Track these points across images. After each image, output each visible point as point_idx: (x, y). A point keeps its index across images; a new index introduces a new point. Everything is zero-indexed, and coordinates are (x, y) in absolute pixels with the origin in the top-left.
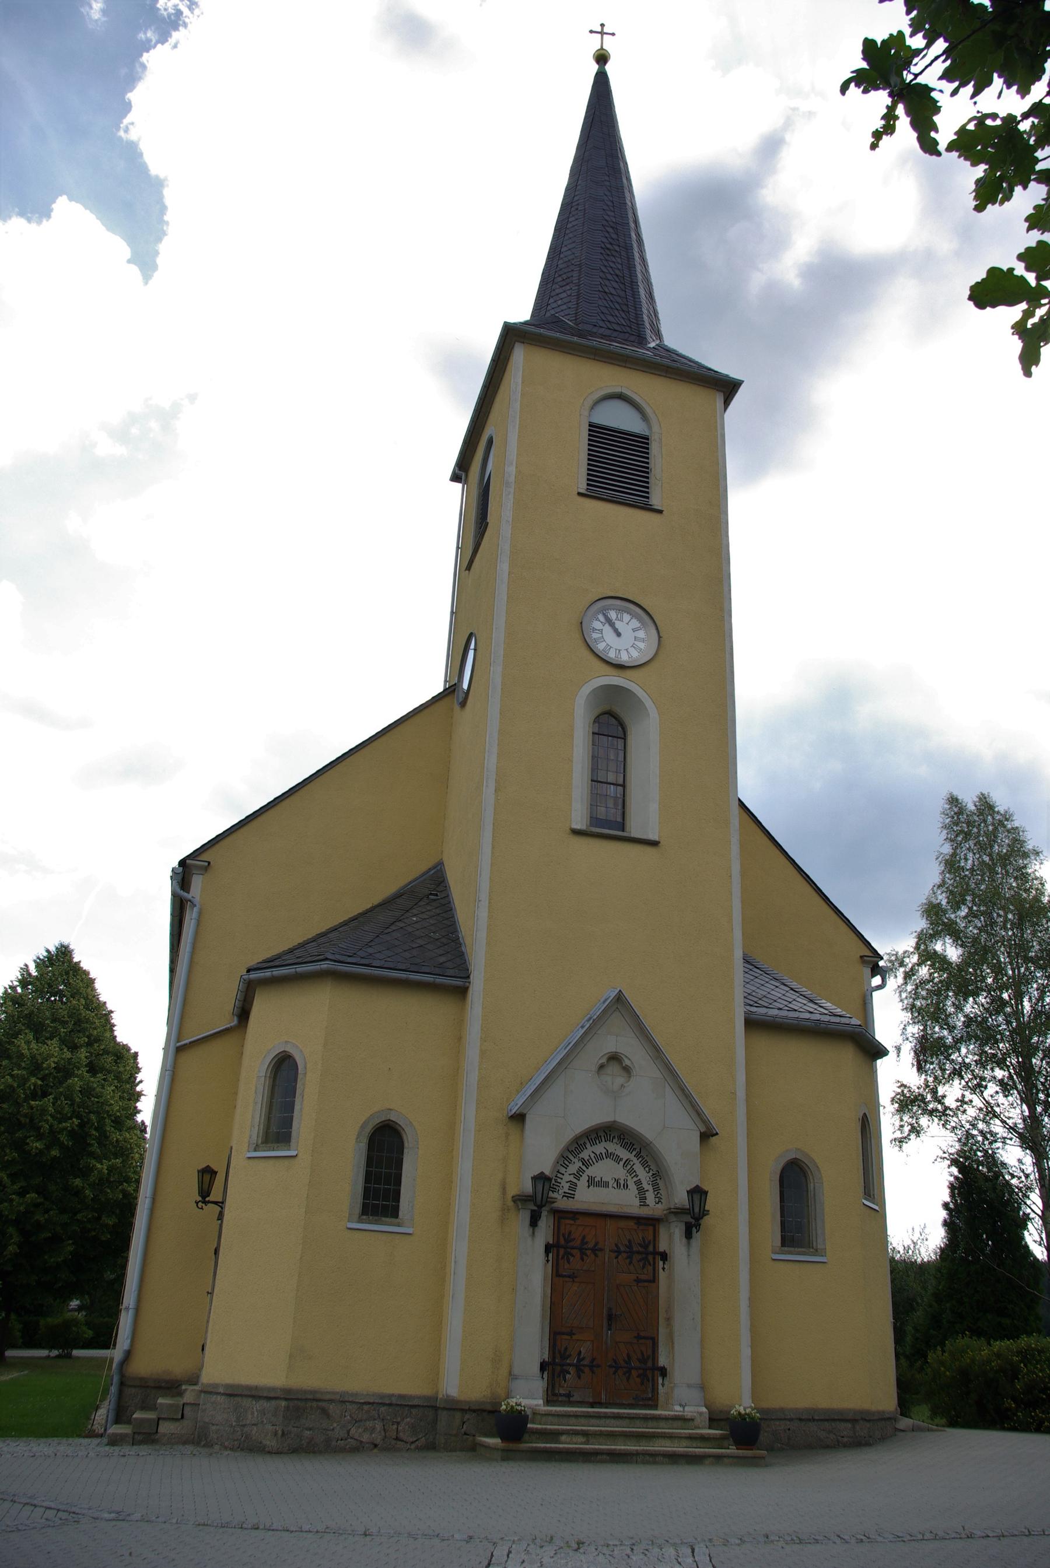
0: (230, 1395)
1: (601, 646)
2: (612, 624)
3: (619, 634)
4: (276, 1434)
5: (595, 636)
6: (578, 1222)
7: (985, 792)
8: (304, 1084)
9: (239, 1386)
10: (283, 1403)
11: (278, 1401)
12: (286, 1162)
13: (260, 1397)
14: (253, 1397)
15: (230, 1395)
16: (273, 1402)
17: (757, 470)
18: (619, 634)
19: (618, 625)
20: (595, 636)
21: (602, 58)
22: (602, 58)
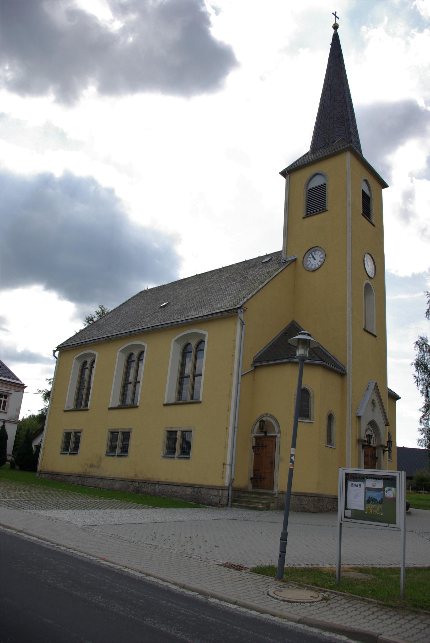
0: (296, 495)
1: (317, 266)
2: (313, 256)
3: (315, 259)
4: (315, 507)
5: (310, 266)
6: (299, 617)
7: (232, 78)
8: (314, 400)
9: (299, 493)
10: (316, 498)
11: (314, 498)
12: (309, 424)
13: (307, 496)
14: (305, 496)
15: (296, 495)
16: (313, 498)
17: (168, 256)
18: (315, 259)
19: (315, 256)
20: (310, 266)
21: (336, 27)
22: (336, 27)
